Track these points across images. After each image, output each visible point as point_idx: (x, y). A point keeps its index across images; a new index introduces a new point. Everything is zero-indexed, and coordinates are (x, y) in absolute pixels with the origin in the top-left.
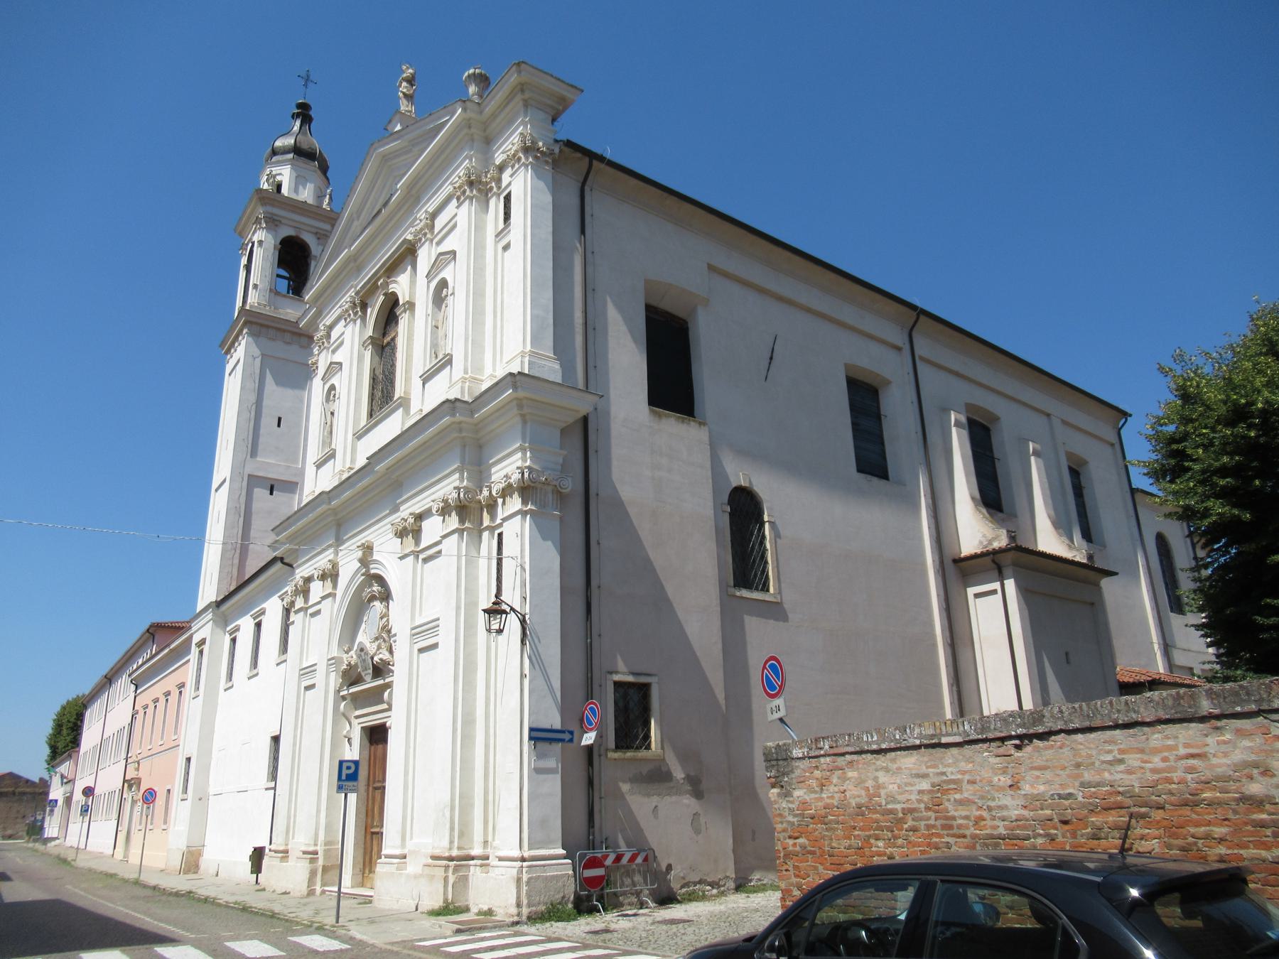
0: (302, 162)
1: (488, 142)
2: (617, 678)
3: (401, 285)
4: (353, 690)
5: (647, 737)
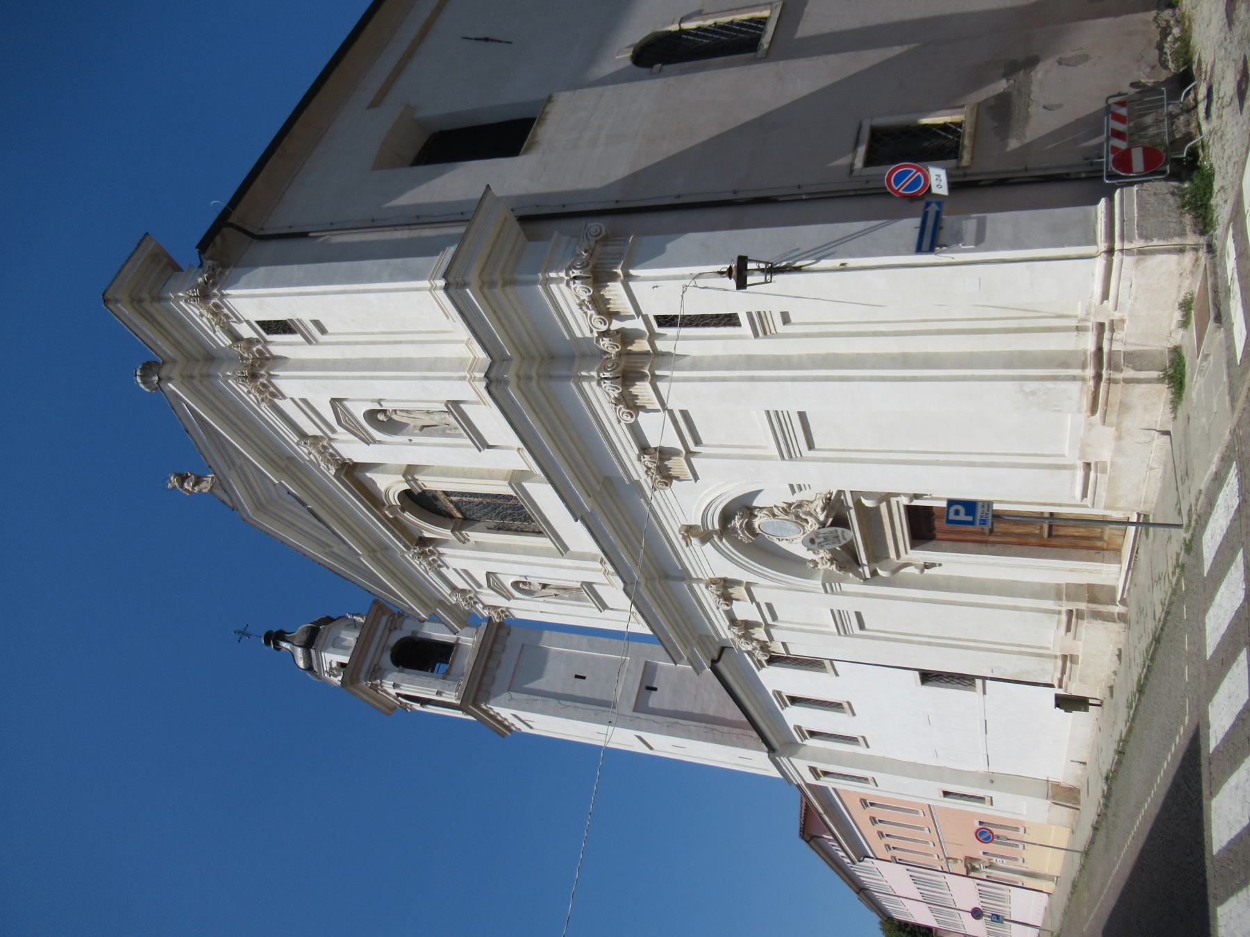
0: (319, 641)
1: (211, 357)
2: (859, 164)
3: (390, 485)
4: (864, 559)
5: (944, 127)
